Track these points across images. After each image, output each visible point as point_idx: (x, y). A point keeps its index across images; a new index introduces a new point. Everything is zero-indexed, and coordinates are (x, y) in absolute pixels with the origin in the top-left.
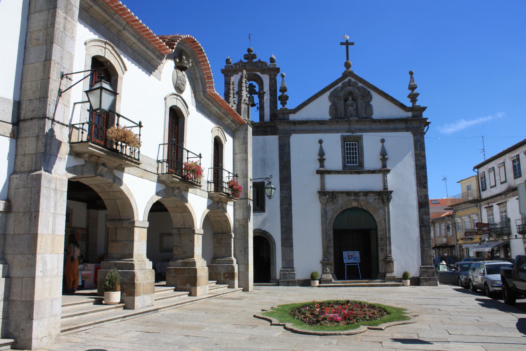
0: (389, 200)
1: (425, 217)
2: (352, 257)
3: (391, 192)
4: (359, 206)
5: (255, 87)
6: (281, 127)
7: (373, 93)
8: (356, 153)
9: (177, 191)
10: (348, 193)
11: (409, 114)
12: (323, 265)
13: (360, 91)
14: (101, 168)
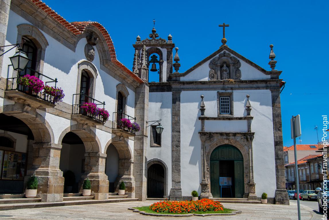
0: (251, 139)
1: (279, 152)
2: (224, 181)
3: (253, 133)
4: (230, 144)
5: (157, 57)
6: (174, 86)
7: (241, 61)
8: (228, 105)
9: (85, 126)
10: (222, 134)
11: (269, 77)
12: (202, 186)
13: (232, 60)
14: (26, 107)
